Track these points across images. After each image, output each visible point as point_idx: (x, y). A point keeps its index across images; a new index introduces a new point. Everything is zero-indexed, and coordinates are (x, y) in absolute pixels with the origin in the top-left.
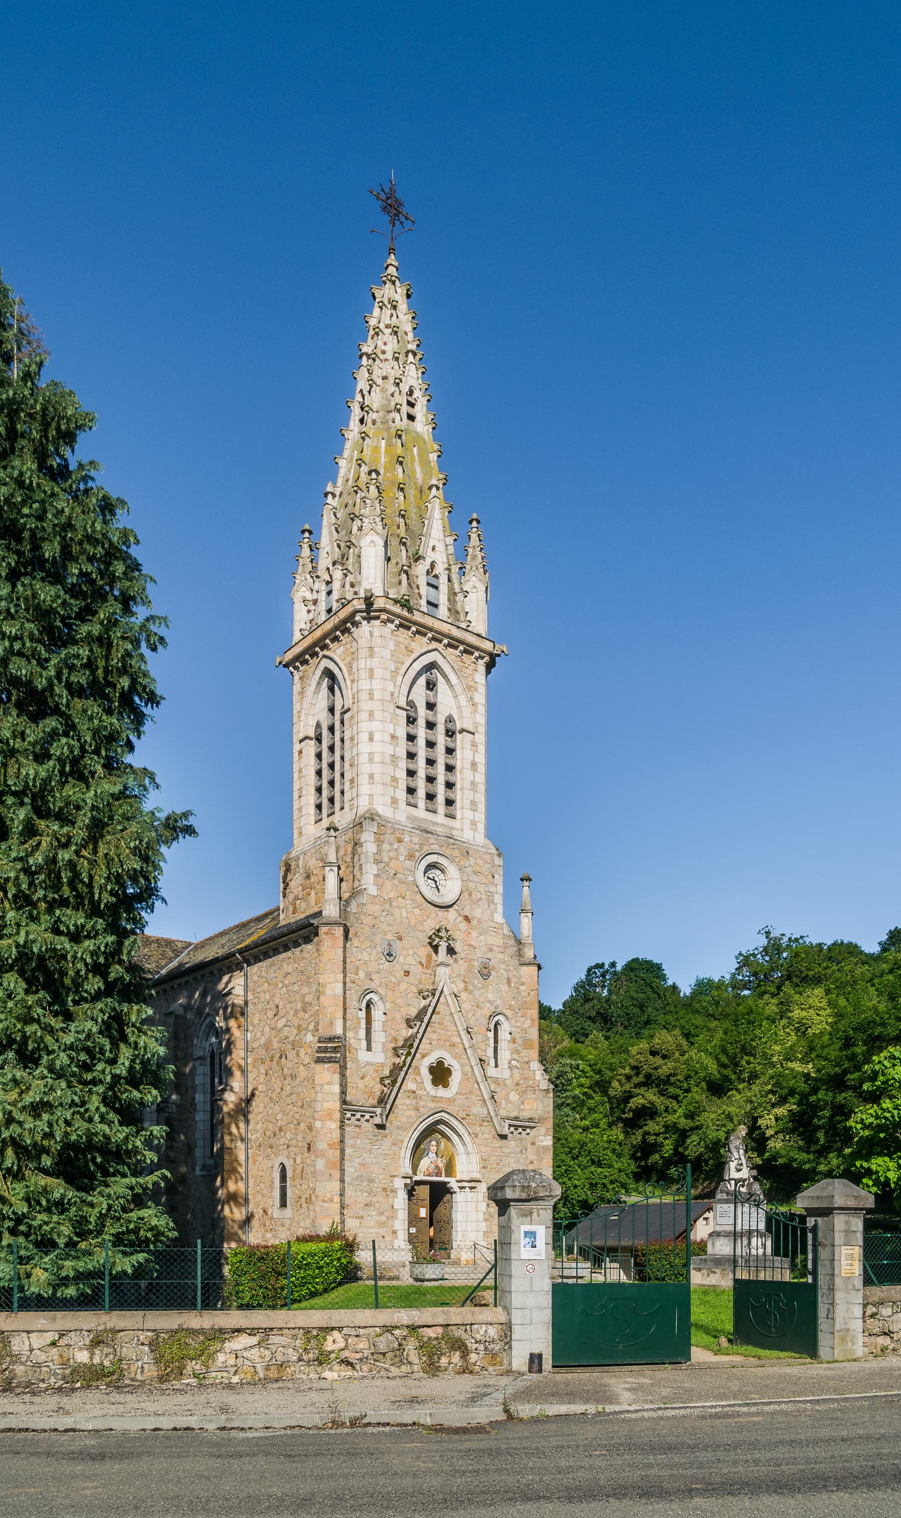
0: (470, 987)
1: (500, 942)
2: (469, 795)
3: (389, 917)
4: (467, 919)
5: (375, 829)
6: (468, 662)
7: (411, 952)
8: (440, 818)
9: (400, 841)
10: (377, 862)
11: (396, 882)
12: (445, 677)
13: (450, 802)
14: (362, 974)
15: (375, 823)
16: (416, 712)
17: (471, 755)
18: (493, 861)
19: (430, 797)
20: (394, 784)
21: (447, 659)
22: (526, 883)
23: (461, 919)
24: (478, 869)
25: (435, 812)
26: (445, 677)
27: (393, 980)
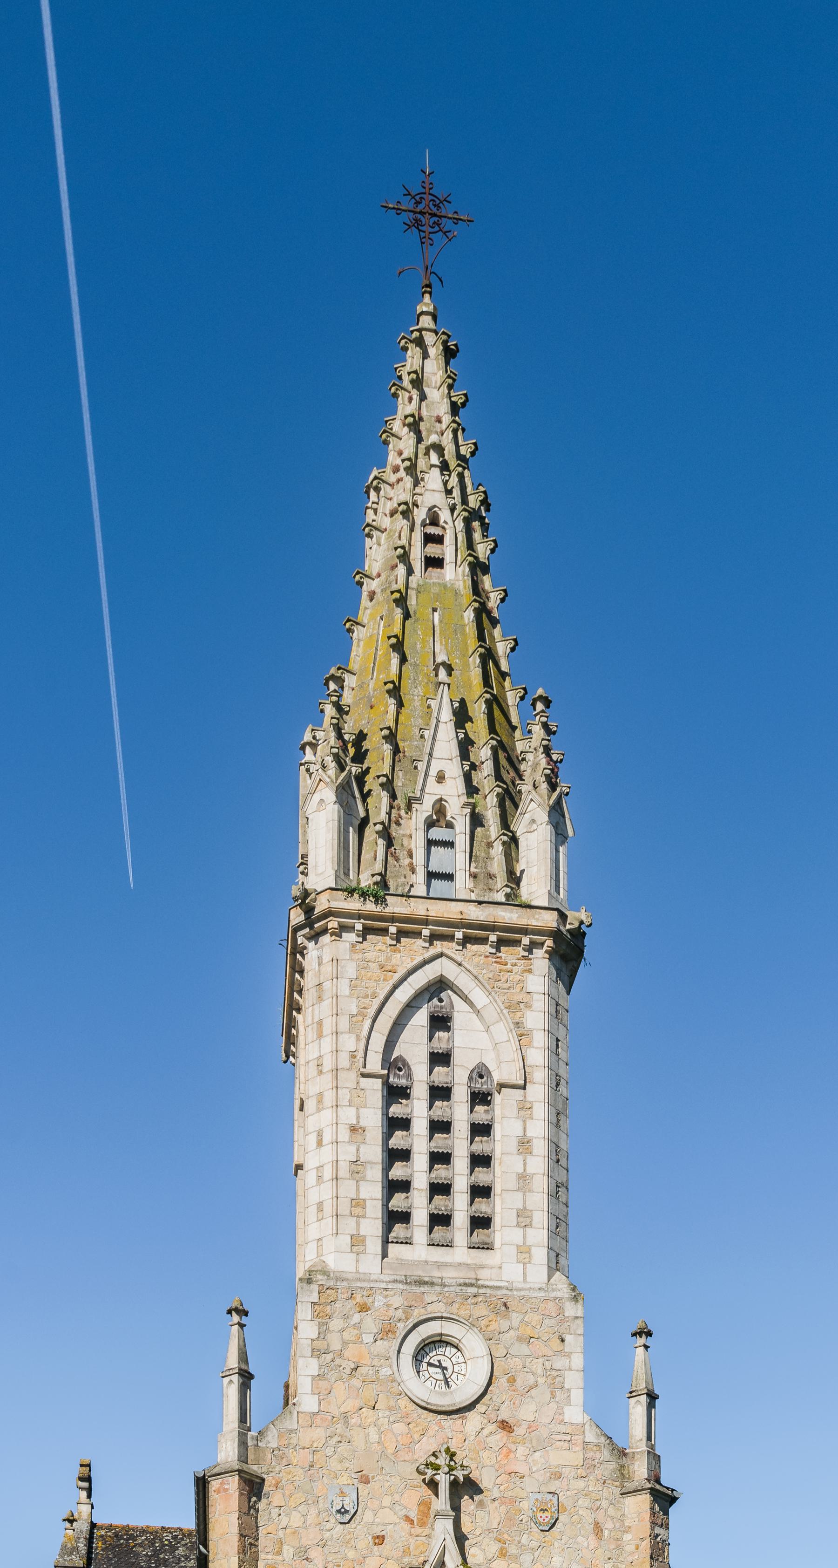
0: (512, 1550)
1: (575, 1457)
2: (516, 1200)
3: (344, 1446)
4: (505, 1426)
5: (314, 1298)
6: (511, 960)
7: (387, 1501)
8: (460, 1253)
9: (364, 1308)
10: (317, 1353)
11: (356, 1382)
12: (465, 999)
13: (480, 1223)
14: (288, 1552)
15: (315, 1287)
16: (409, 1076)
17: (521, 1130)
18: (561, 1310)
19: (440, 1220)
20: (358, 1211)
21: (461, 966)
22: (641, 1341)
23: (492, 1427)
24: (529, 1332)
25: (449, 1245)
26: (465, 999)
27: (351, 1554)
